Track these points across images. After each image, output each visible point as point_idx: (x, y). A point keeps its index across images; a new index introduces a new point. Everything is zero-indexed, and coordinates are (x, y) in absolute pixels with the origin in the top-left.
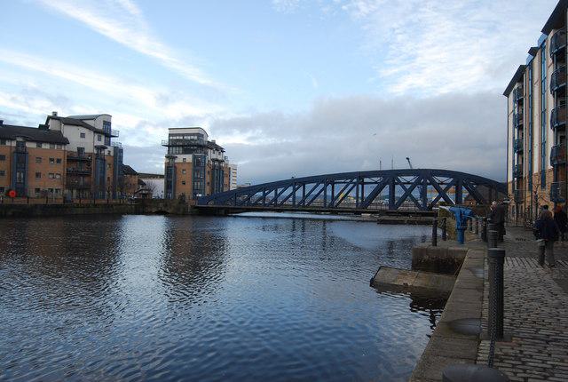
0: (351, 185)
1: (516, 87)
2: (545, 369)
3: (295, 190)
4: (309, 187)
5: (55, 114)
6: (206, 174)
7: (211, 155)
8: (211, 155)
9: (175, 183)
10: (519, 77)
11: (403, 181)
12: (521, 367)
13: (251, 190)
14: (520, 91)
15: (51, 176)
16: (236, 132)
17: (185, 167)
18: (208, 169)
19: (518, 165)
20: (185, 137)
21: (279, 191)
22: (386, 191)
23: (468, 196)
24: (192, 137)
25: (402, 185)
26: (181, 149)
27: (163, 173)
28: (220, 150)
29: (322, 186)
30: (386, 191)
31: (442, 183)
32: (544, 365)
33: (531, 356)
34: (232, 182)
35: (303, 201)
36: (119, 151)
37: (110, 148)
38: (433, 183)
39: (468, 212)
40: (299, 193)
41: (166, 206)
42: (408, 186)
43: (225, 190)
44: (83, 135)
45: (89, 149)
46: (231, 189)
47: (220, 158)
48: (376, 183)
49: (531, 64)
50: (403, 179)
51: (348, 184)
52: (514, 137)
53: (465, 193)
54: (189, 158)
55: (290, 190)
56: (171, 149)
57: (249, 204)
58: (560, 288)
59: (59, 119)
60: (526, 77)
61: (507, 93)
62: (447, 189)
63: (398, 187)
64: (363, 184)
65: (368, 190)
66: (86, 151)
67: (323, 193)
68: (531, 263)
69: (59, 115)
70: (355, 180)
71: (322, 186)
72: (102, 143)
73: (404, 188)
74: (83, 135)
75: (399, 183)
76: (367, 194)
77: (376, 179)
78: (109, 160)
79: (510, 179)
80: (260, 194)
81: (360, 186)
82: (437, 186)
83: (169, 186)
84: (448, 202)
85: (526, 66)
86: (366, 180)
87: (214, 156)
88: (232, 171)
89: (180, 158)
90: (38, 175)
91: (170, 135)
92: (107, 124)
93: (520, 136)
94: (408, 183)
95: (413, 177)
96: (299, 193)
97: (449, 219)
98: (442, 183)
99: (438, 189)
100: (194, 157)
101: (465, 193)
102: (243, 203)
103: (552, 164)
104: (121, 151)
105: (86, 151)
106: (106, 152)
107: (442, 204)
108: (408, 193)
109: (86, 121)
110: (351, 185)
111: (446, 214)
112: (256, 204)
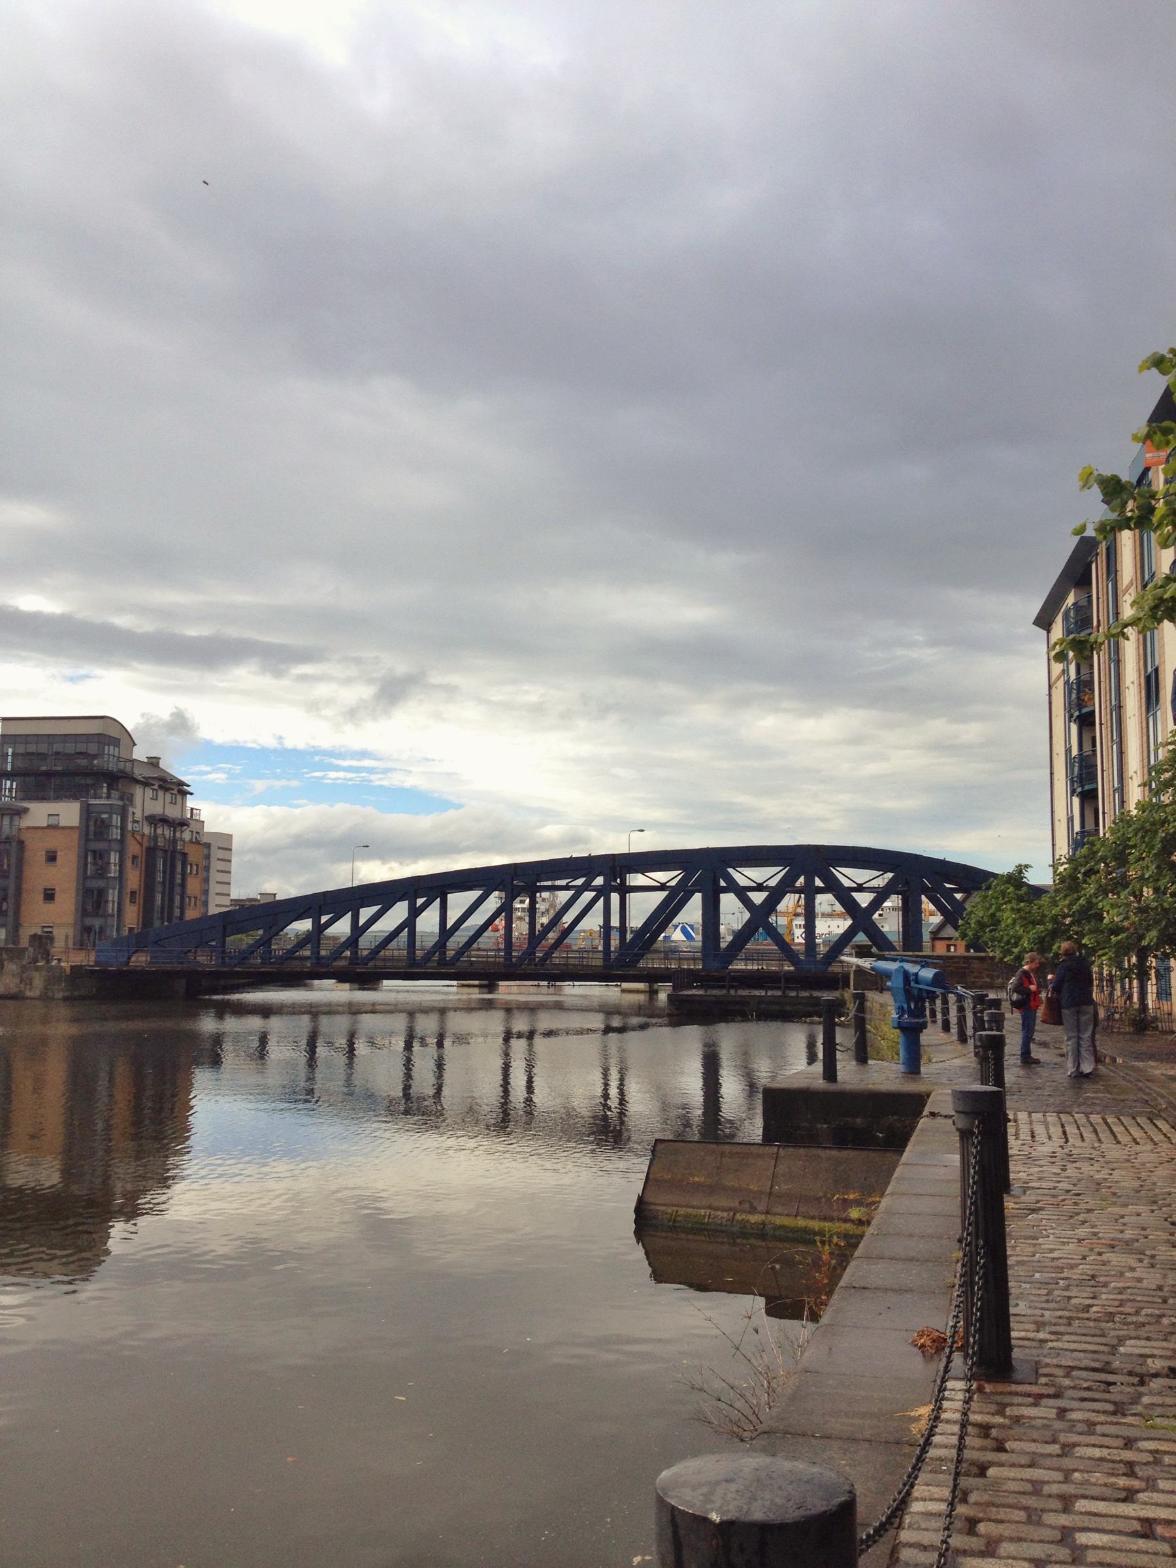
0: (588, 896)
1: (1071, 600)
2: (1130, 1469)
3: (415, 912)
4: (459, 902)
6: (128, 863)
8: (145, 803)
11: (742, 881)
12: (1056, 1462)
14: (1082, 619)
18: (133, 848)
19: (1083, 833)
21: (366, 914)
22: (693, 911)
23: (941, 927)
25: (741, 893)
29: (494, 901)
30: (693, 911)
31: (860, 888)
32: (1128, 1455)
33: (1091, 1424)
34: (214, 888)
35: (441, 945)
38: (833, 886)
39: (928, 973)
40: (428, 922)
42: (758, 898)
43: (191, 914)
46: (213, 910)
47: (172, 812)
48: (662, 887)
50: (745, 876)
51: (579, 891)
52: (1068, 751)
53: (932, 918)
54: (69, 813)
55: (399, 912)
57: (267, 957)
58: (97, 1200)
60: (1098, 571)
62: (876, 904)
63: (729, 902)
64: (624, 890)
65: (642, 907)
67: (500, 922)
68: (1118, 1129)
70: (599, 881)
71: (494, 901)
73: (747, 903)
75: (733, 887)
76: (636, 920)
77: (661, 876)
80: (304, 926)
81: (615, 898)
82: (844, 896)
84: (879, 943)
88: (216, 853)
93: (1087, 747)
94: (760, 887)
95: (773, 870)
96: (428, 922)
97: (874, 998)
98: (860, 888)
99: (851, 907)
100: (87, 813)
101: (932, 918)
102: (244, 956)
107: (862, 952)
108: (760, 917)
110: (588, 896)
111: (877, 981)
112: (290, 954)
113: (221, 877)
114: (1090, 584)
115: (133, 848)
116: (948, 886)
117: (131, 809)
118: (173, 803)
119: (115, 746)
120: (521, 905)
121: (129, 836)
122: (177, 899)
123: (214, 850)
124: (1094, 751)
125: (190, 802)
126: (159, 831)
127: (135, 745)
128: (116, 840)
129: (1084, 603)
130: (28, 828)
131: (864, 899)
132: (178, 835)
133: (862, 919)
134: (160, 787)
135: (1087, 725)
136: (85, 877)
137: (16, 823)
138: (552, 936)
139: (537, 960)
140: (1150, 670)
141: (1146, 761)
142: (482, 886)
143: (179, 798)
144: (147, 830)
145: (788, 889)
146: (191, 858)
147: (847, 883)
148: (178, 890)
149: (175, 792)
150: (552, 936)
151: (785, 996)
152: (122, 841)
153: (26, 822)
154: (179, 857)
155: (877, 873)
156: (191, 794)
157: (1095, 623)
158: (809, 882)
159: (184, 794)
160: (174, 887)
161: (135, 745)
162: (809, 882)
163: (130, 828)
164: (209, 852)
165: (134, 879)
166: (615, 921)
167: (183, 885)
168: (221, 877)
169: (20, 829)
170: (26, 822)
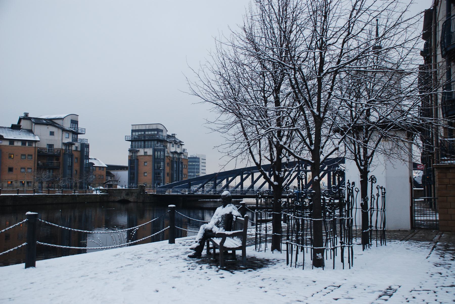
3: (243, 180)
5: (26, 114)
7: (172, 148)
9: (138, 173)
15: (23, 170)
16: (445, 19)
17: (147, 158)
18: (167, 161)
20: (147, 133)
24: (153, 133)
27: (126, 164)
28: (180, 144)
36: (85, 146)
37: (77, 144)
44: (52, 133)
45: (58, 145)
47: (179, 151)
54: (150, 152)
55: (238, 179)
56: (134, 143)
59: (30, 119)
66: (168, 241)
69: (30, 116)
72: (70, 140)
74: (52, 133)
78: (76, 155)
83: (133, 178)
87: (173, 150)
88: (201, 161)
89: (141, 152)
90: (11, 170)
91: (133, 131)
92: (75, 122)
104: (88, 146)
105: (168, 241)
106: (74, 148)
109: (56, 121)
113: (203, 168)
115: (167, 161)
117: (166, 150)
118: (179, 147)
119: (75, 124)
121: (166, 158)
122: (180, 175)
123: (200, 159)
126: (175, 156)
128: (162, 159)
130: (139, 156)
132: (180, 157)
134: (175, 143)
136: (155, 169)
137: (136, 155)
143: (180, 146)
144: (171, 155)
146: (184, 163)
148: (180, 172)
149: (179, 144)
152: (164, 159)
153: (139, 154)
154: (180, 163)
159: (182, 145)
160: (179, 172)
163: (166, 155)
165: (167, 170)
167: (182, 171)
168: (203, 168)
169: (137, 156)
170: (139, 154)
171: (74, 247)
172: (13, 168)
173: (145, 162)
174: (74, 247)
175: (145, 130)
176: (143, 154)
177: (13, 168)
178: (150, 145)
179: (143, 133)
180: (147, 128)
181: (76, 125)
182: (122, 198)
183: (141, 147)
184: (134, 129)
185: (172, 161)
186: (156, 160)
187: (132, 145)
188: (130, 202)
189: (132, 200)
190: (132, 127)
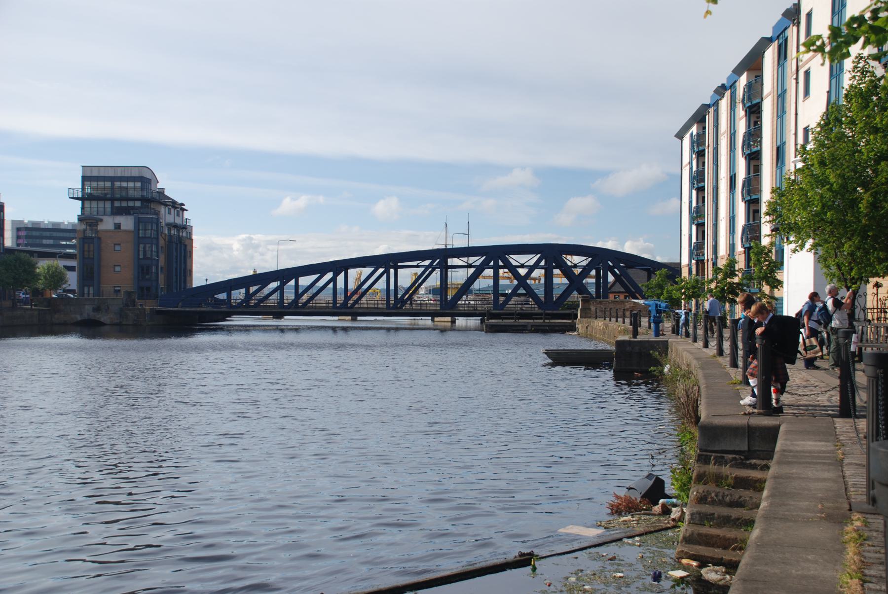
10: (699, 118)
13: (229, 285)
20: (117, 184)
26: (108, 205)
28: (179, 208)
29: (329, 275)
31: (522, 266)
38: (508, 265)
41: (97, 309)
47: (178, 221)
49: (716, 104)
54: (127, 223)
56: (87, 204)
61: (680, 136)
66: (80, 214)
71: (329, 275)
79: (685, 261)
82: (567, 271)
83: (88, 275)
85: (709, 106)
86: (141, 257)
89: (108, 224)
91: (85, 179)
103: (743, 246)
114: (705, 122)
116: (622, 265)
120: (341, 278)
124: (704, 169)
125: (186, 215)
127: (158, 182)
129: (701, 132)
131: (523, 272)
133: (523, 281)
134: (173, 207)
135: (701, 156)
136: (139, 259)
138: (355, 298)
139: (391, 305)
140: (732, 173)
141: (728, 214)
142: (374, 265)
143: (181, 212)
145: (485, 267)
147: (514, 263)
150: (355, 298)
151: (544, 322)
153: (101, 227)
155: (585, 258)
156: (187, 210)
157: (707, 145)
158: (496, 263)
159: (184, 210)
161: (158, 182)
162: (496, 263)
164: (17, 241)
166: (392, 287)
171: (625, 281)
172: (120, 223)
173: (115, 244)
174: (625, 281)
175: (113, 179)
176: (111, 227)
177: (120, 223)
178: (102, 210)
179: (108, 184)
180: (119, 175)
181: (833, 99)
182: (85, 316)
183: (105, 214)
184: (88, 174)
185: (170, 240)
186: (139, 239)
187: (83, 208)
188: (103, 324)
189: (108, 321)
190: (83, 171)
